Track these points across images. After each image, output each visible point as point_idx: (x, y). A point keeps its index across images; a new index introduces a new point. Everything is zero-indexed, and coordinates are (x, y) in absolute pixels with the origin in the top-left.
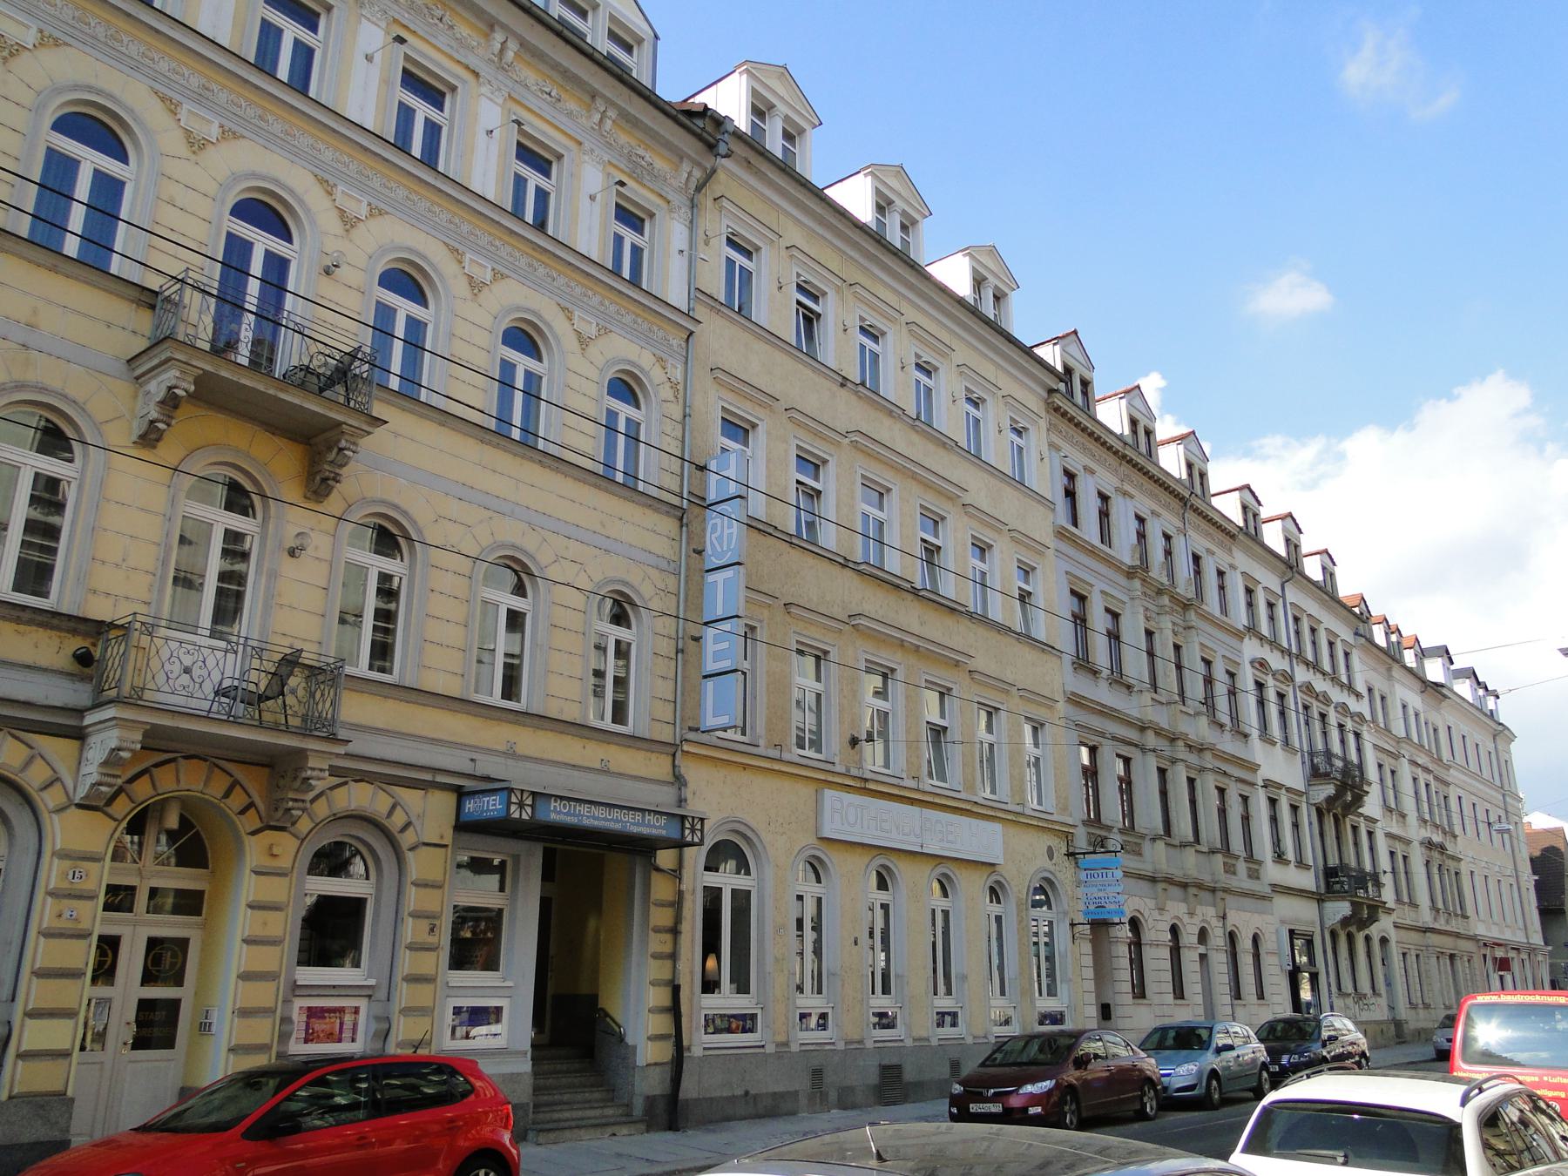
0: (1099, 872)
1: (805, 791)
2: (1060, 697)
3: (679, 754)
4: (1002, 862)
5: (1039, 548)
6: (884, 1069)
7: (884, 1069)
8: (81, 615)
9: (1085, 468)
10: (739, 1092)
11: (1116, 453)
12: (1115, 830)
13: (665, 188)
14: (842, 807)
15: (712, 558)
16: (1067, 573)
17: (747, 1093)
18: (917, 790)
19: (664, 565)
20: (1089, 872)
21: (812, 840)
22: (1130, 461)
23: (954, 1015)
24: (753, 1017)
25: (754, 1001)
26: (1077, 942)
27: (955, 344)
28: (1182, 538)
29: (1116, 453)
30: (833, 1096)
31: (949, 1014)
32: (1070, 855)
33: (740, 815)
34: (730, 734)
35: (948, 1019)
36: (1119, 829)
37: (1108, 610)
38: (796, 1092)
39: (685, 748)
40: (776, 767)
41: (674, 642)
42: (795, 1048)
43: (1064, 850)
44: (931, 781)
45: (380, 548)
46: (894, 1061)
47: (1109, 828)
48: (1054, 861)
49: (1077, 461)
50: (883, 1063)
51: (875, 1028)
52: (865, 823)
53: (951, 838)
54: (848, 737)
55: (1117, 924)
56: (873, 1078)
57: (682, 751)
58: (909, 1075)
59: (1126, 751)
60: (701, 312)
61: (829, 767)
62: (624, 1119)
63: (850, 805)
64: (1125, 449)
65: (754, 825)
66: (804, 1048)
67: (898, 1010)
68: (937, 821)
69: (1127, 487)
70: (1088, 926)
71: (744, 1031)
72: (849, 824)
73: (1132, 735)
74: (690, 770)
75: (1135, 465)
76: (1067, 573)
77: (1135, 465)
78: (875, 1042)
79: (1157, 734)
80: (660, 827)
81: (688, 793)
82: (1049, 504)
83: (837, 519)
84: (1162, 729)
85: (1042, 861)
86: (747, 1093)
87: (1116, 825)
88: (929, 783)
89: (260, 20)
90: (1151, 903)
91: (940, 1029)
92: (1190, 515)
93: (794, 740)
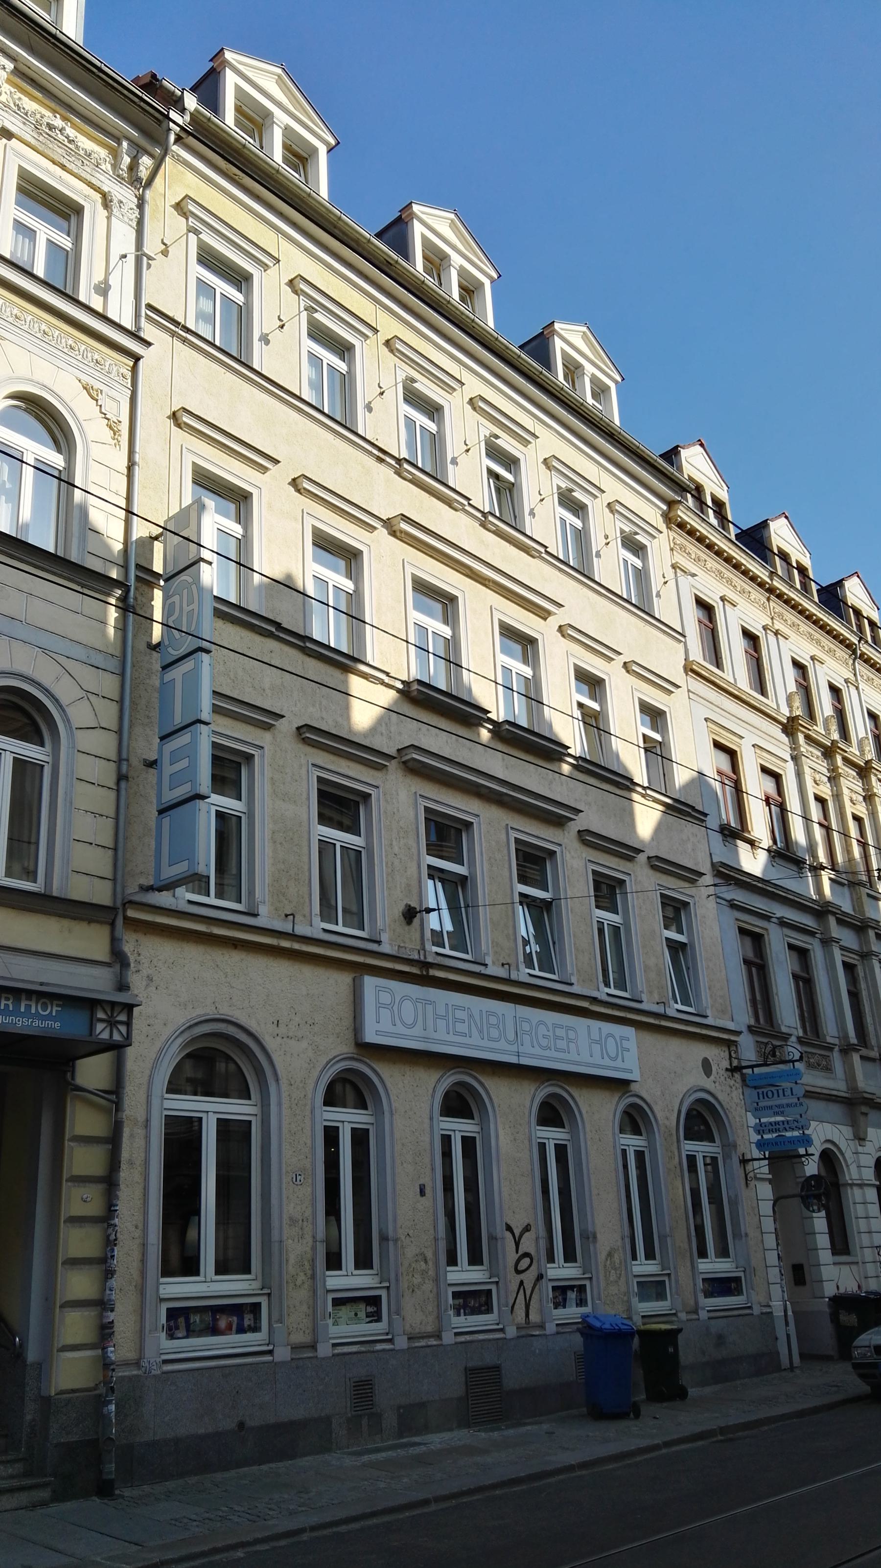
0: (765, 1090)
1: (342, 980)
2: (705, 868)
3: (120, 921)
4: (638, 1079)
5: (667, 686)
6: (471, 1372)
7: (471, 1372)
8: (63, 896)
9: (723, 599)
10: (229, 1424)
11: (761, 585)
12: (793, 1039)
13: (98, 175)
14: (393, 1001)
15: (170, 650)
16: (706, 719)
17: (241, 1425)
18: (292, 936)
19: (99, 660)
20: (760, 1091)
21: (347, 1048)
22: (780, 596)
23: (582, 1289)
24: (255, 1308)
25: (256, 1285)
26: (752, 1184)
27: (539, 429)
28: (852, 689)
29: (761, 585)
30: (390, 1420)
31: (572, 1288)
32: (733, 1070)
33: (225, 1011)
34: (185, 896)
35: (572, 1295)
36: (798, 1038)
37: (765, 770)
38: (327, 1420)
39: (131, 913)
40: (285, 944)
41: (113, 766)
42: (324, 1350)
43: (726, 1064)
44: (607, 990)
45: (328, 812)
46: (489, 1359)
47: (785, 1037)
48: (712, 1077)
49: (712, 591)
50: (470, 1364)
51: (459, 1315)
52: (430, 1023)
53: (562, 1044)
54: (401, 907)
55: (803, 1156)
56: (455, 1387)
57: (126, 918)
58: (512, 1380)
59: (799, 940)
60: (149, 331)
61: (373, 947)
62: (15, 1483)
63: (405, 998)
64: (772, 580)
65: (252, 1025)
66: (339, 1350)
67: (494, 1288)
68: (541, 1022)
69: (778, 625)
70: (766, 1162)
71: (241, 1330)
72: (404, 1024)
73: (807, 921)
74: (130, 944)
75: (787, 601)
76: (706, 719)
77: (787, 601)
78: (456, 1334)
79: (840, 922)
80: (49, 1017)
81: (136, 981)
82: (680, 635)
83: (304, 600)
84: (845, 914)
85: (698, 1079)
86: (241, 1425)
87: (794, 1032)
88: (675, 1008)
89: (17, 167)
90: (847, 1131)
91: (560, 1311)
92: (860, 666)
93: (521, 958)
